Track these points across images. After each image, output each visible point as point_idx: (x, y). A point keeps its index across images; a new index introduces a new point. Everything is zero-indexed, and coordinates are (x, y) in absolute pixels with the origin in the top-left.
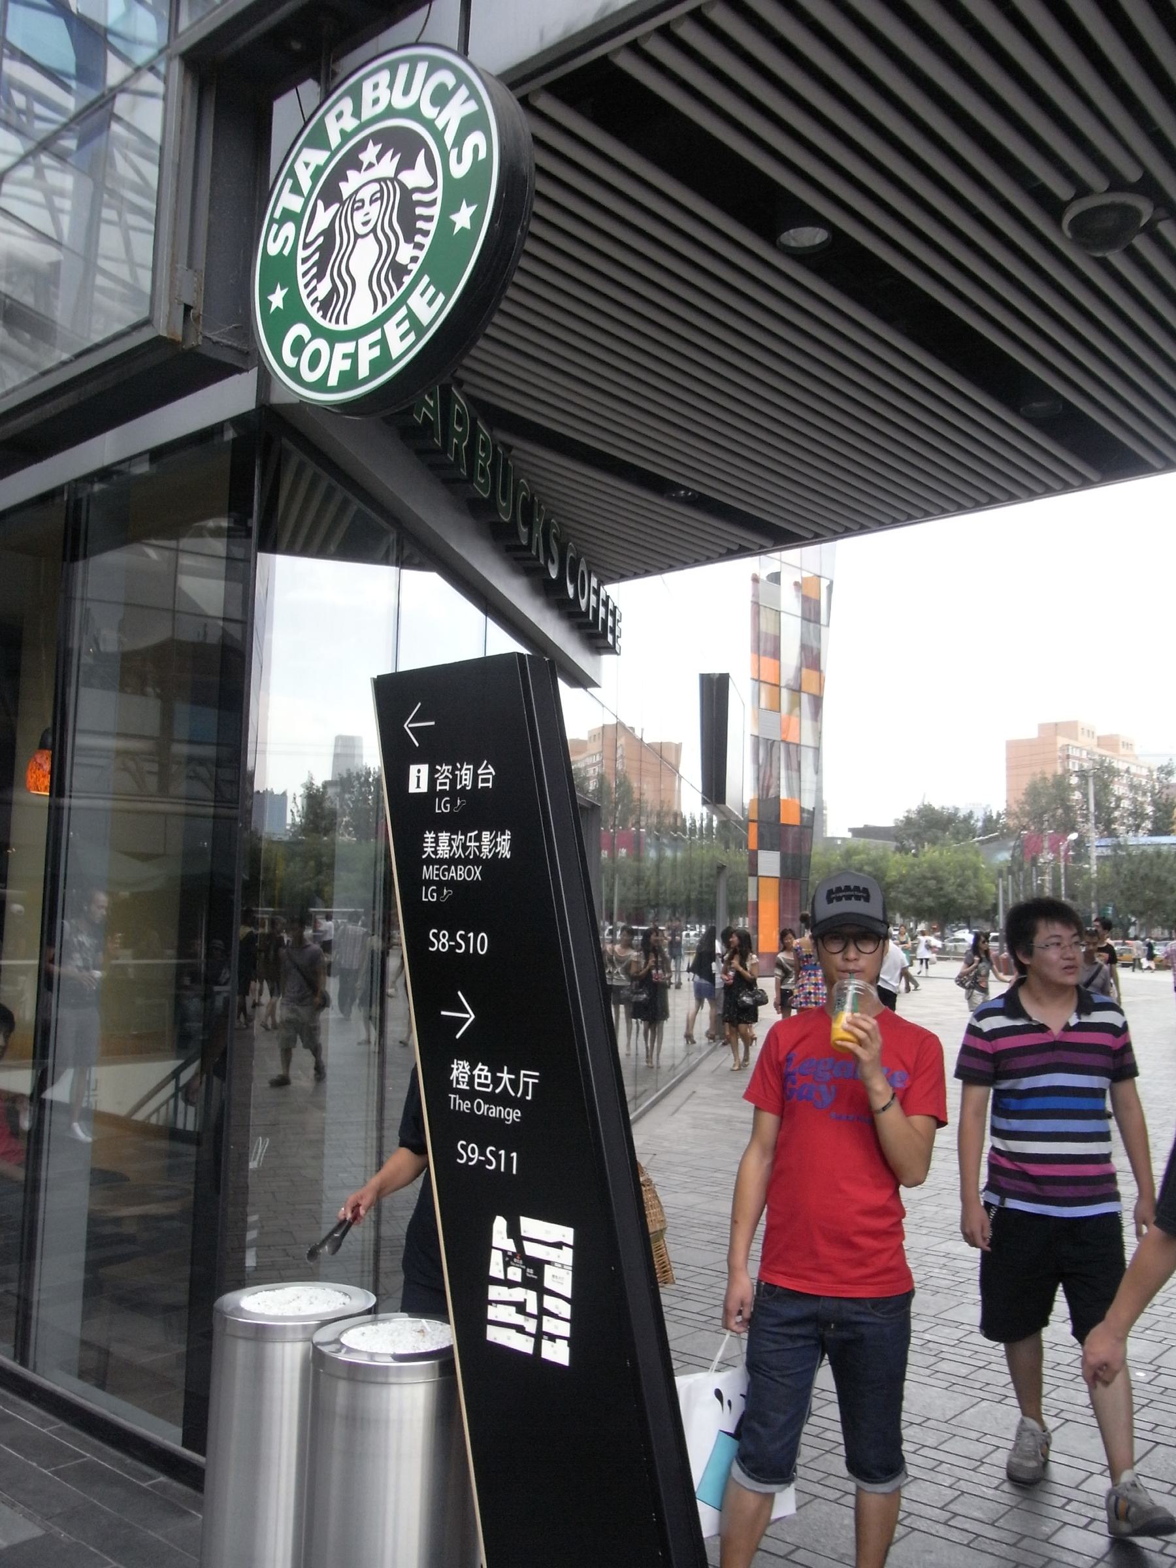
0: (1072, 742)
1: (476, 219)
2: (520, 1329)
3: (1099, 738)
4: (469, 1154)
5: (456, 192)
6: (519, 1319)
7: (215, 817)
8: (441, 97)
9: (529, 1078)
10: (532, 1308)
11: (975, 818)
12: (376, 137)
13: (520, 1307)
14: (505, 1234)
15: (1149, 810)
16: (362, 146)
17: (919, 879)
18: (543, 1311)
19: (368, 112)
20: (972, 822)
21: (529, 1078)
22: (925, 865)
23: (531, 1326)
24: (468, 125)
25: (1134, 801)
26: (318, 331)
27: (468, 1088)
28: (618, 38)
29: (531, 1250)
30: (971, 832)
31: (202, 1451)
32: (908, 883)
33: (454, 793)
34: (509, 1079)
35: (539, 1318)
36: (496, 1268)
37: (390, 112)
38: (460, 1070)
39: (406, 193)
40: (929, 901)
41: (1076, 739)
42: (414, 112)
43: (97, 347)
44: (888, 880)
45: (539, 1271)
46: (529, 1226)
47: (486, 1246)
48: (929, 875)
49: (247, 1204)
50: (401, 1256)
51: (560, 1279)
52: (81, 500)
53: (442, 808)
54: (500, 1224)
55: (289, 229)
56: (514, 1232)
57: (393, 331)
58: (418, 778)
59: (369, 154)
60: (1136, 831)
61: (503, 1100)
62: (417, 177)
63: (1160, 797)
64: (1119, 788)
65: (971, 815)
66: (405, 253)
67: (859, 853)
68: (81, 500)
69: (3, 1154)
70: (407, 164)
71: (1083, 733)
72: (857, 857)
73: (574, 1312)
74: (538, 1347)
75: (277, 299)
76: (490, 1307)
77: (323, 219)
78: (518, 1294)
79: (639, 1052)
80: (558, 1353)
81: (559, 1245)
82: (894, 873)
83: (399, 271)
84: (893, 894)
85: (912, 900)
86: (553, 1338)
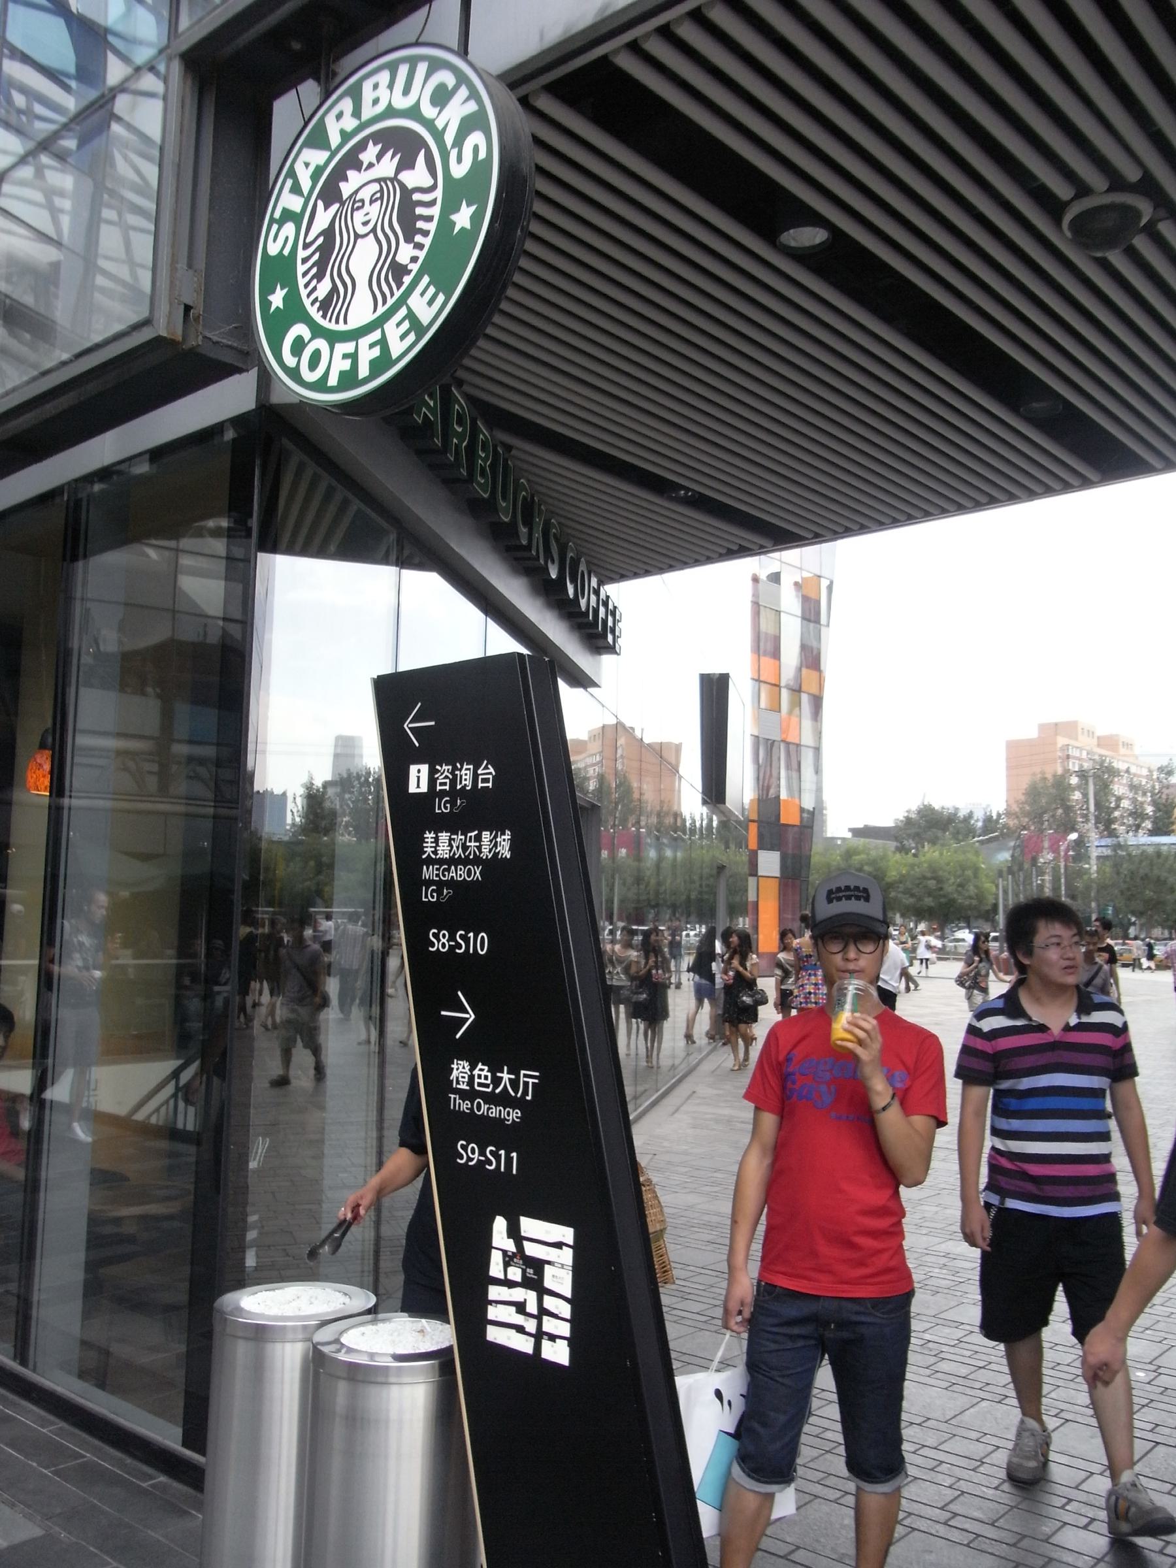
0: (1072, 742)
1: (476, 219)
2: (520, 1329)
3: (1099, 738)
4: (469, 1154)
5: (456, 192)
6: (519, 1319)
7: (215, 817)
8: (441, 97)
9: (529, 1078)
10: (532, 1308)
11: (975, 818)
12: (376, 137)
13: (520, 1307)
14: (505, 1234)
15: (1149, 810)
16: (362, 146)
17: (919, 879)
18: (543, 1311)
19: (368, 112)
20: (972, 822)
21: (529, 1078)
22: (925, 865)
23: (531, 1326)
24: (468, 125)
25: (1134, 801)
26: (318, 331)
27: (468, 1088)
28: (618, 38)
29: (531, 1250)
30: (971, 832)
31: (202, 1451)
32: (908, 883)
33: (454, 793)
34: (509, 1079)
35: (539, 1318)
36: (496, 1268)
37: (390, 112)
38: (460, 1070)
39: (406, 193)
40: (929, 901)
41: (1076, 739)
42: (414, 112)
43: (97, 347)
44: (888, 880)
45: (539, 1271)
46: (529, 1226)
47: (486, 1246)
48: (929, 875)
49: (247, 1204)
50: (401, 1256)
51: (560, 1279)
52: (81, 500)
53: (442, 808)
54: (500, 1224)
55: (289, 229)
56: (514, 1232)
57: (393, 331)
58: (418, 778)
59: (369, 154)
60: (1136, 831)
61: (503, 1100)
62: (417, 177)
63: (1160, 797)
64: (1119, 788)
65: (971, 815)
66: (405, 253)
67: (859, 853)
68: (81, 500)
69: (3, 1154)
70: (407, 164)
71: (1083, 733)
72: (857, 857)
73: (574, 1312)
74: (538, 1347)
75: (277, 299)
76: (490, 1307)
77: (323, 219)
78: (518, 1294)
79: (639, 1052)
80: (558, 1353)
81: (559, 1245)
82: (894, 873)
83: (399, 271)
84: (893, 894)
85: (912, 900)
86: (553, 1338)
